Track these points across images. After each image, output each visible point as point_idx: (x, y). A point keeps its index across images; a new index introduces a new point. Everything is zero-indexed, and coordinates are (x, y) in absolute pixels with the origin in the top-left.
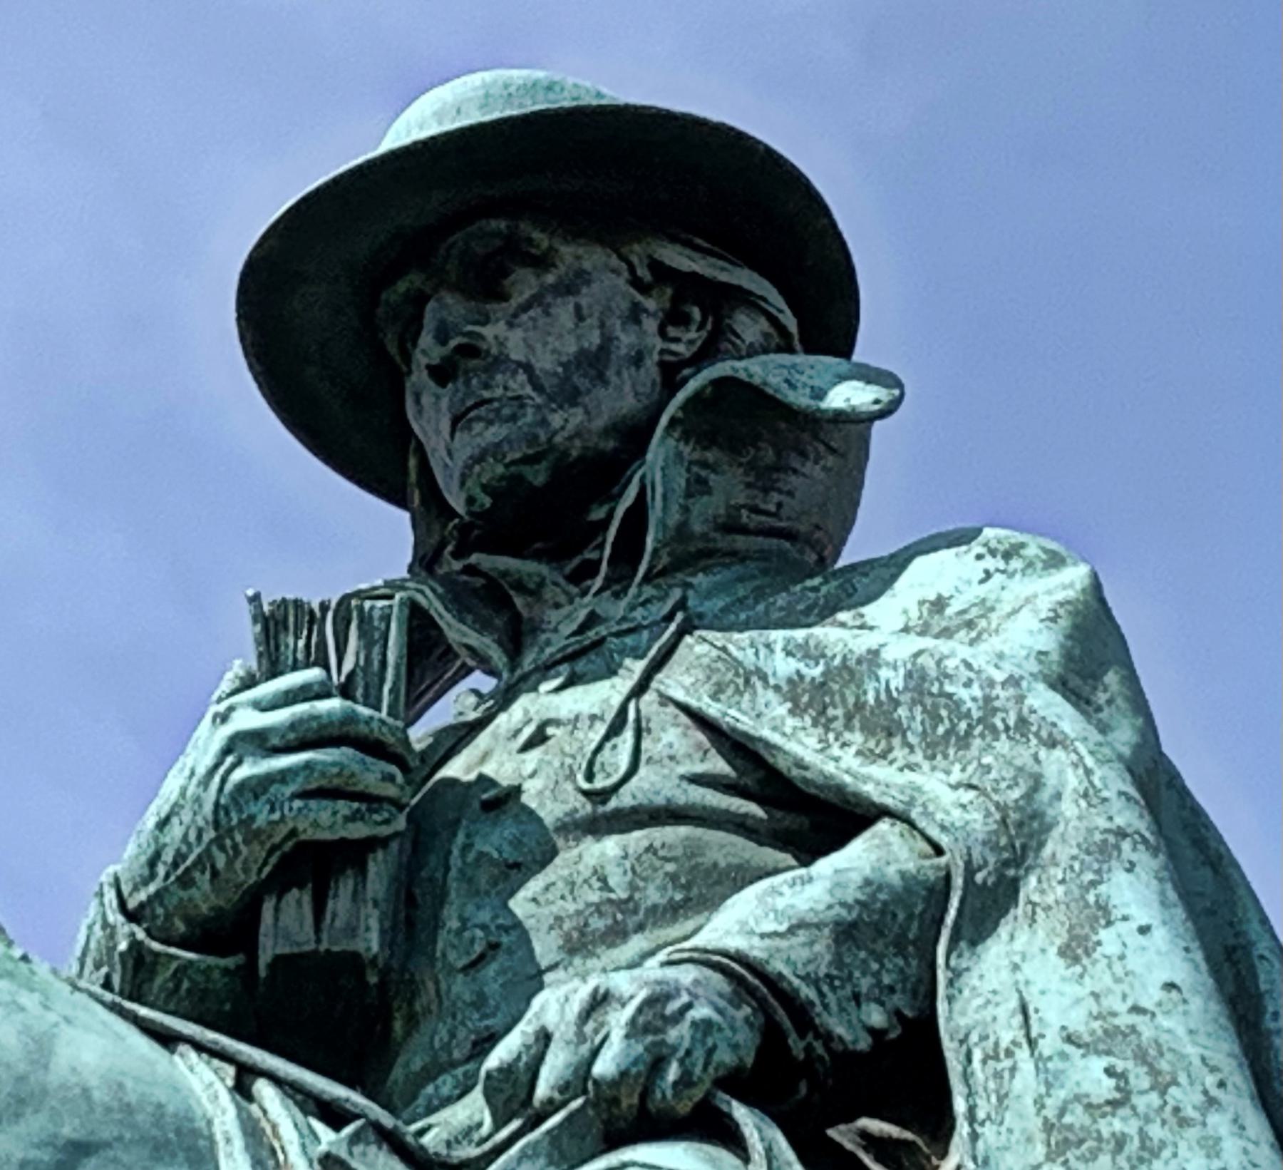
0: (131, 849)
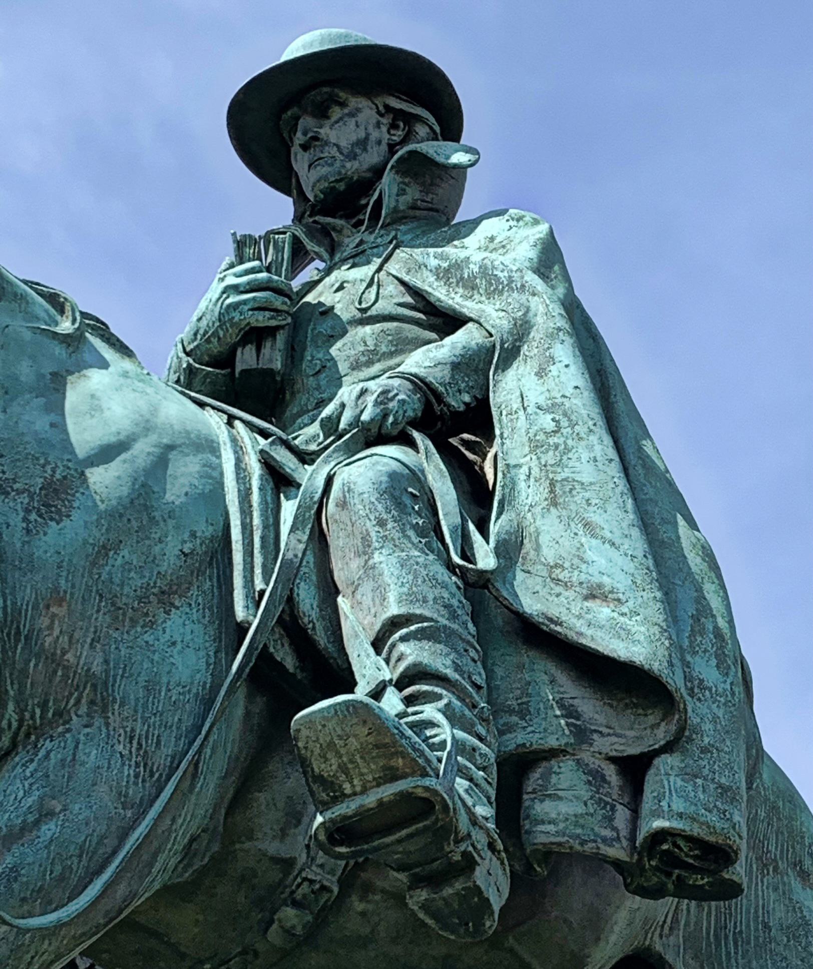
0: (187, 329)
